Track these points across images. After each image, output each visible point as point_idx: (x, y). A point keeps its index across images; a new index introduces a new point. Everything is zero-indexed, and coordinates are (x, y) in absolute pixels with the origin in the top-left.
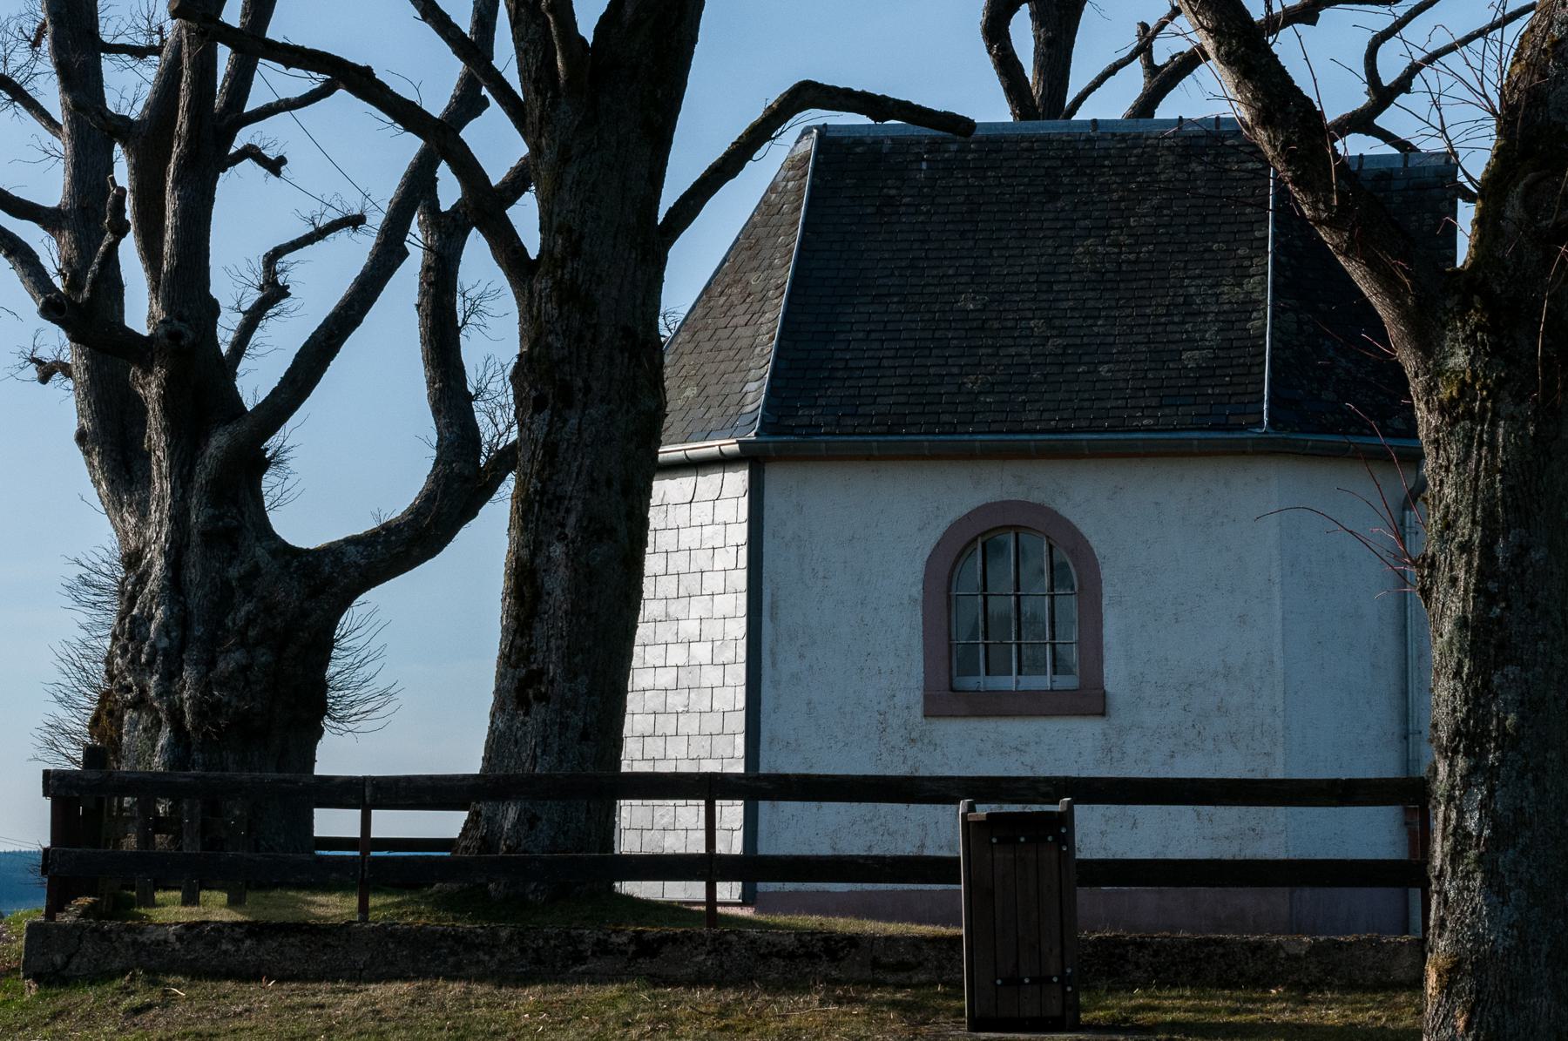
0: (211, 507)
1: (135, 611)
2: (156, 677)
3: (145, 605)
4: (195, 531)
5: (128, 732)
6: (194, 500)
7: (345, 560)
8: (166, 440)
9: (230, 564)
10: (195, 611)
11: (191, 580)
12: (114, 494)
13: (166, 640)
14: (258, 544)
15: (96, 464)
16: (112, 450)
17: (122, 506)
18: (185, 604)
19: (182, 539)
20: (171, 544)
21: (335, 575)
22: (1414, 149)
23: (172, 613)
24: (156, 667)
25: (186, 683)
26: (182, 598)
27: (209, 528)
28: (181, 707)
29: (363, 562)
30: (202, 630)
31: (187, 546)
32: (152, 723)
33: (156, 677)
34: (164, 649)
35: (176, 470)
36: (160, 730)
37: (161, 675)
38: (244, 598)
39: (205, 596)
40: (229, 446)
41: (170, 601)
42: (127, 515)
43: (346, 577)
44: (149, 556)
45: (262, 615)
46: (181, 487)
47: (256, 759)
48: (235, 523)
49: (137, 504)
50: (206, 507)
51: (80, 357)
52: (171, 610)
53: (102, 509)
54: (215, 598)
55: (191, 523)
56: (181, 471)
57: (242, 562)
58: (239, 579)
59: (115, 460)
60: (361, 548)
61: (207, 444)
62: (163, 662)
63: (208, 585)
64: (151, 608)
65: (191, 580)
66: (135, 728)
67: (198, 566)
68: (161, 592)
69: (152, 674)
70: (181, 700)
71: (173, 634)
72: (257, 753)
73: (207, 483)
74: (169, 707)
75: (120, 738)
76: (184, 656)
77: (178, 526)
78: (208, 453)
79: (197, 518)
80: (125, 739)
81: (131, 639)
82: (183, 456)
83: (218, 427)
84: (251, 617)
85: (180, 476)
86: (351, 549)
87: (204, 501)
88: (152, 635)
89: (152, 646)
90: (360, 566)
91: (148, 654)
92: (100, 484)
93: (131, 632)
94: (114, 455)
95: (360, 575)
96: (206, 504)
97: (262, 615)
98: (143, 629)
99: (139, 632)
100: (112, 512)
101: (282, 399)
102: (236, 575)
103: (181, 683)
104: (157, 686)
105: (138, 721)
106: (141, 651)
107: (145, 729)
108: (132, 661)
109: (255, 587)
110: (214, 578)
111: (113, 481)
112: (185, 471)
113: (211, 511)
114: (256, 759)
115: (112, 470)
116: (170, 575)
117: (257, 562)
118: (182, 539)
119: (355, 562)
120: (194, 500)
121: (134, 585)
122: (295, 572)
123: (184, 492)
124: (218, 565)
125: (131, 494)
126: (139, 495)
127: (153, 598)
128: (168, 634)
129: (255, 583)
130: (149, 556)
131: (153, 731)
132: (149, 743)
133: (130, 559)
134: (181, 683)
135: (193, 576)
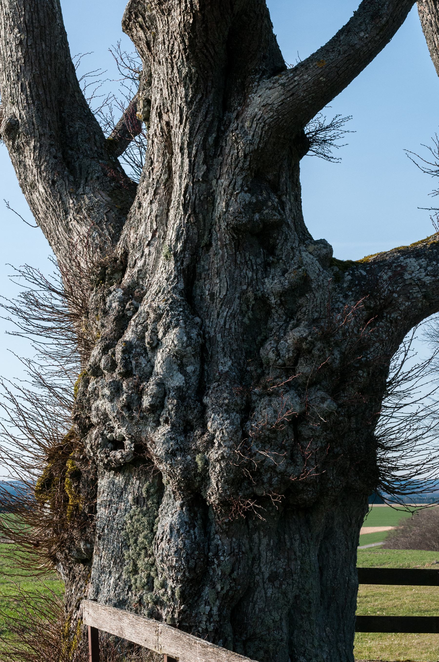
0: (249, 191)
1: (129, 335)
2: (164, 429)
3: (145, 328)
4: (223, 225)
5: (109, 504)
6: (224, 181)
7: (407, 276)
8: (186, 95)
9: (266, 273)
10: (219, 336)
11: (212, 295)
12: (55, 197)
13: (180, 376)
14: (303, 248)
15: (29, 162)
16: (51, 145)
17: (66, 212)
18: (202, 326)
19: (200, 236)
20: (185, 243)
21: (395, 295)
22: (208, 250)
23: (189, 338)
24: (164, 414)
25: (213, 437)
26: (197, 319)
27: (244, 220)
28: (205, 470)
29: (428, 280)
30: (230, 363)
31: (209, 245)
32: (148, 491)
33: (164, 429)
34: (179, 389)
35: (199, 138)
36: (159, 503)
37: (173, 426)
38: (287, 322)
39: (233, 316)
40: (283, 103)
41: (185, 322)
42: (75, 223)
43: (408, 299)
44: (140, 263)
45: (319, 345)
46: (204, 162)
47: (297, 544)
48: (277, 217)
49: (89, 210)
50: (242, 190)
51: (12, 30)
52: (188, 334)
53: (33, 221)
54: (246, 320)
55: (217, 214)
56: (205, 140)
57: (284, 272)
58: (281, 295)
59: (55, 157)
60: (423, 262)
61: (244, 104)
62: (177, 407)
63: (237, 301)
64: (155, 332)
65: (212, 295)
66: (120, 497)
67: (223, 276)
68: (171, 309)
69: (158, 424)
70: (206, 462)
71: (190, 369)
72: (297, 536)
73: (245, 156)
74: (186, 470)
75: (93, 510)
76: (206, 400)
77: (196, 217)
78: (250, 111)
79: (227, 205)
80: (102, 512)
81: (127, 374)
82: (209, 119)
83: (260, 79)
84: (304, 346)
85: (204, 146)
86: (412, 262)
87: (240, 182)
88: (158, 368)
89: (160, 384)
90: (424, 285)
91: (153, 396)
92: (33, 186)
93: (126, 363)
94: (53, 150)
95: (425, 297)
96: (242, 186)
97: (319, 345)
98: (143, 361)
99: (138, 365)
100: (50, 224)
101: (361, 39)
102: (278, 288)
103: (206, 437)
104: (167, 441)
105: (125, 489)
106: (140, 393)
107: (137, 501)
108: (128, 407)
109: (301, 306)
110: (244, 292)
111: (54, 182)
112: (211, 140)
113: (247, 197)
114: (297, 544)
115: (53, 169)
116: (181, 286)
117: (305, 271)
118: (200, 236)
119: (419, 280)
120: (224, 181)
121: (122, 302)
122: (349, 288)
123: (208, 170)
124: (250, 274)
125: (78, 197)
126: (90, 198)
127: (159, 317)
128: (182, 368)
129: (301, 301)
130: (140, 263)
131: (149, 502)
132: (145, 520)
133: (104, 268)
134: (206, 437)
135: (216, 288)
